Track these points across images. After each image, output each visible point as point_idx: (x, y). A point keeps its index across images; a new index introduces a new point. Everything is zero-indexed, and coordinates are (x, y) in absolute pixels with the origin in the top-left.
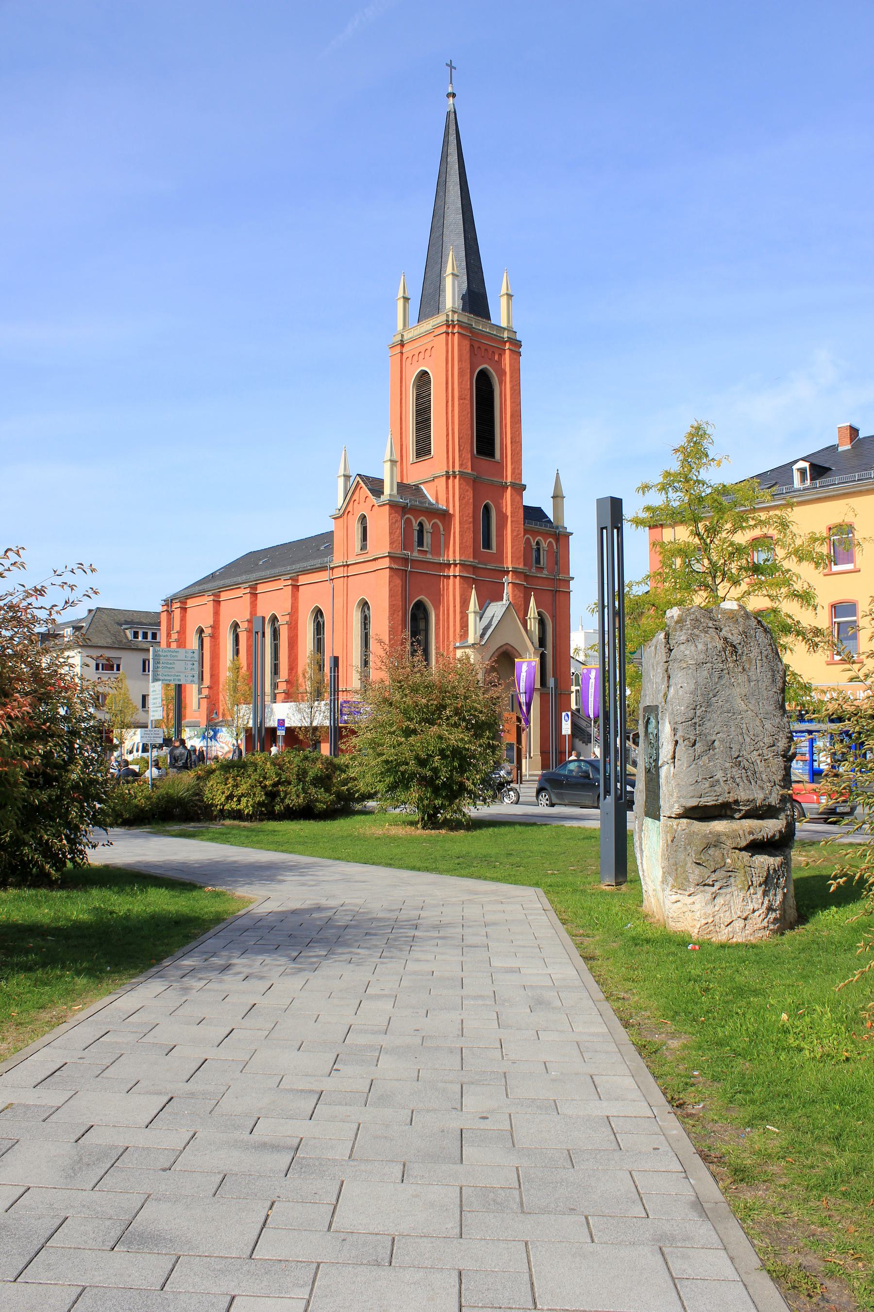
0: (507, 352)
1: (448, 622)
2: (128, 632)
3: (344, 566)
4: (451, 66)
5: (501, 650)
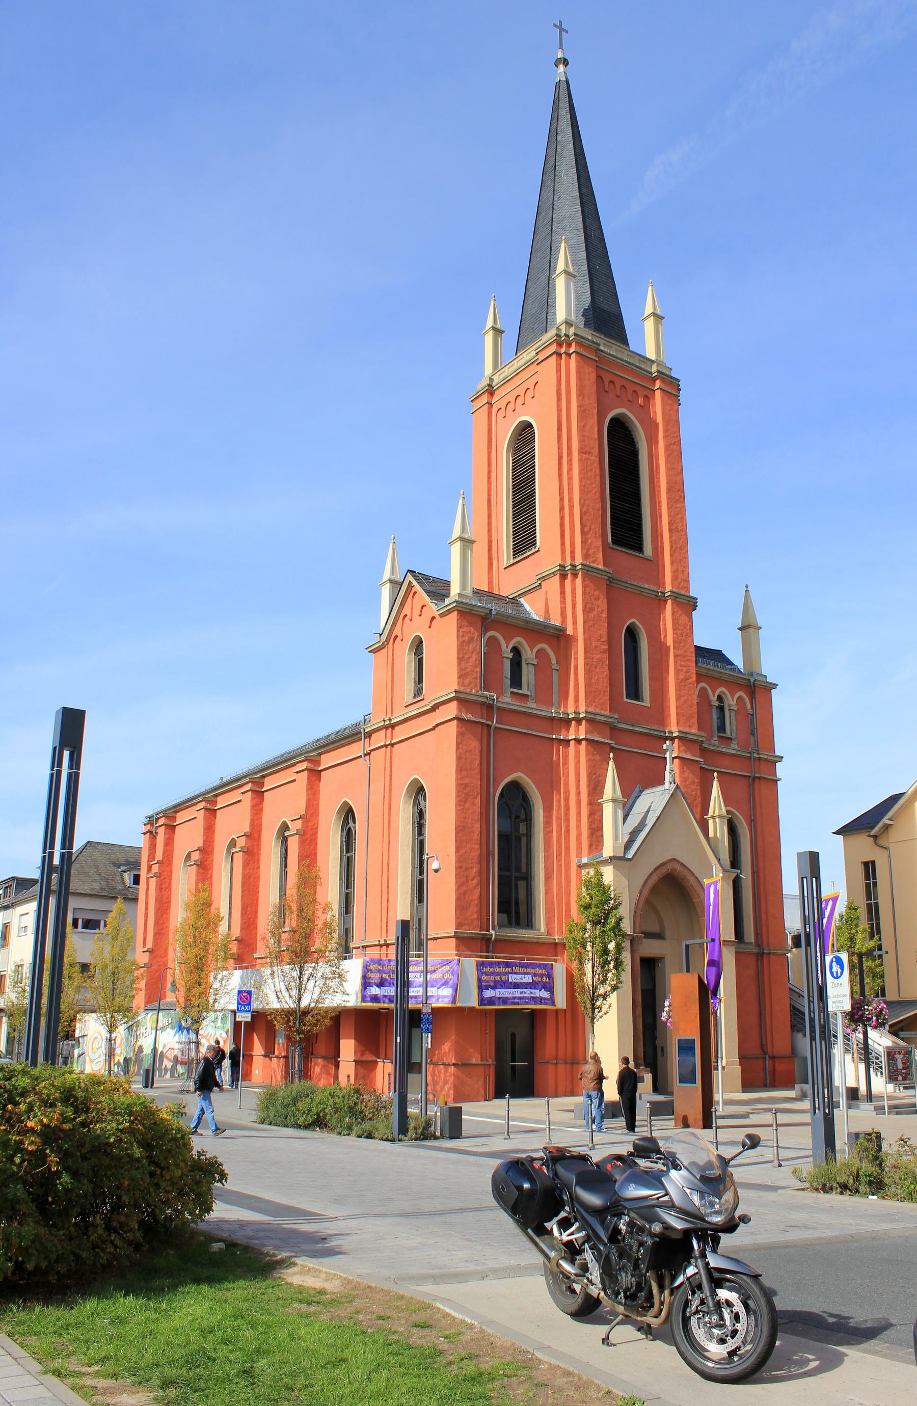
0: (658, 394)
1: (567, 820)
2: (126, 875)
3: (386, 727)
4: (560, 27)
5: (664, 870)
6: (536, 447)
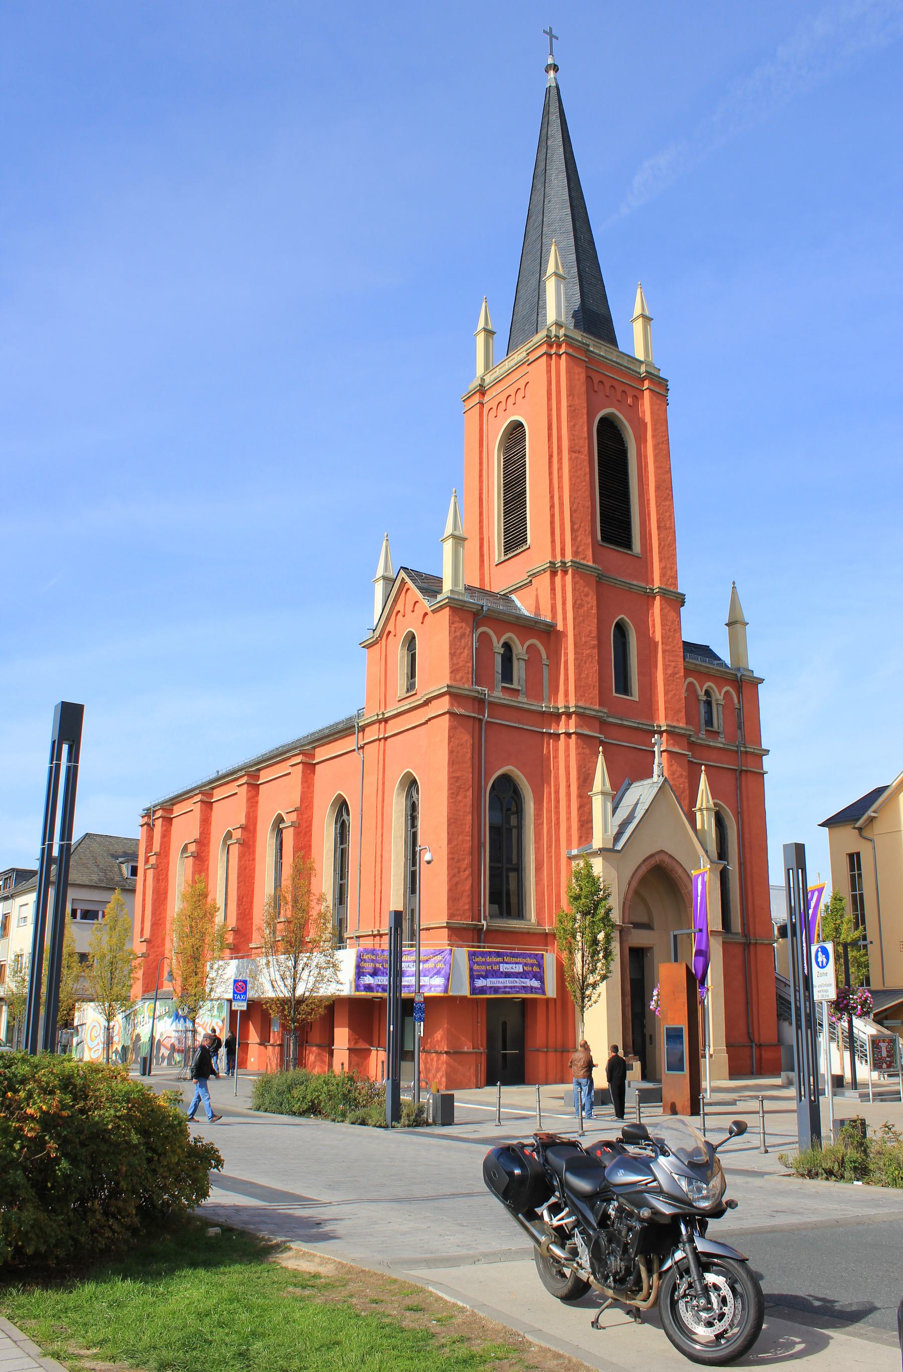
1: (558, 813)
2: (124, 866)
4: (550, 33)
5: (652, 862)
6: (527, 446)
